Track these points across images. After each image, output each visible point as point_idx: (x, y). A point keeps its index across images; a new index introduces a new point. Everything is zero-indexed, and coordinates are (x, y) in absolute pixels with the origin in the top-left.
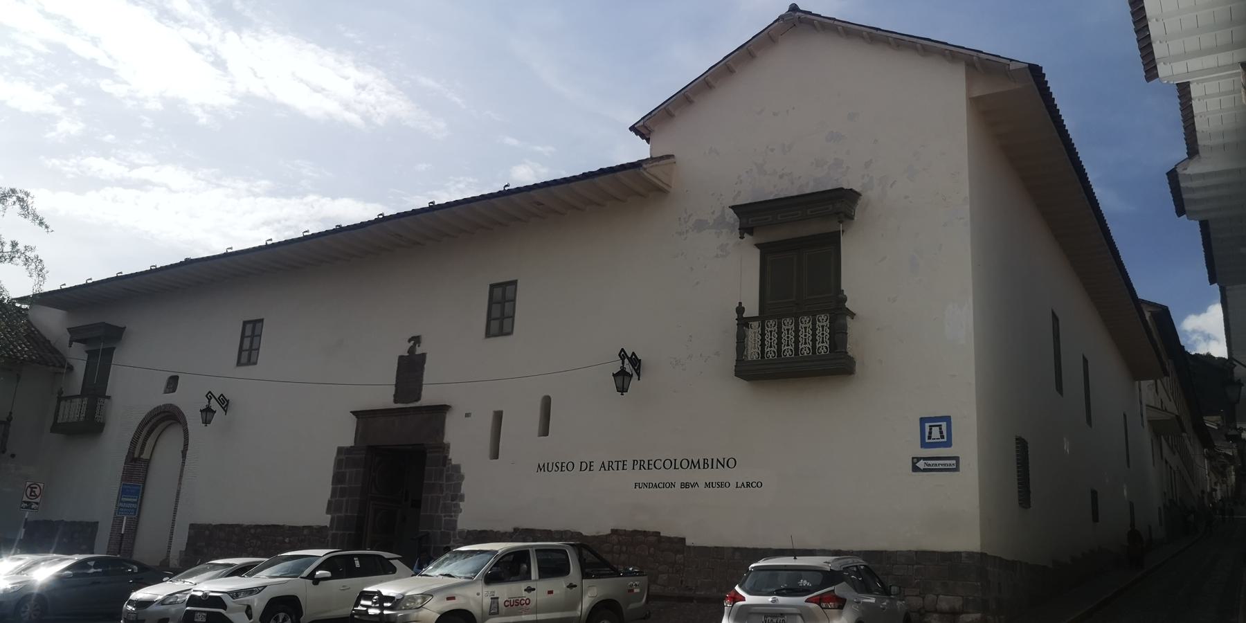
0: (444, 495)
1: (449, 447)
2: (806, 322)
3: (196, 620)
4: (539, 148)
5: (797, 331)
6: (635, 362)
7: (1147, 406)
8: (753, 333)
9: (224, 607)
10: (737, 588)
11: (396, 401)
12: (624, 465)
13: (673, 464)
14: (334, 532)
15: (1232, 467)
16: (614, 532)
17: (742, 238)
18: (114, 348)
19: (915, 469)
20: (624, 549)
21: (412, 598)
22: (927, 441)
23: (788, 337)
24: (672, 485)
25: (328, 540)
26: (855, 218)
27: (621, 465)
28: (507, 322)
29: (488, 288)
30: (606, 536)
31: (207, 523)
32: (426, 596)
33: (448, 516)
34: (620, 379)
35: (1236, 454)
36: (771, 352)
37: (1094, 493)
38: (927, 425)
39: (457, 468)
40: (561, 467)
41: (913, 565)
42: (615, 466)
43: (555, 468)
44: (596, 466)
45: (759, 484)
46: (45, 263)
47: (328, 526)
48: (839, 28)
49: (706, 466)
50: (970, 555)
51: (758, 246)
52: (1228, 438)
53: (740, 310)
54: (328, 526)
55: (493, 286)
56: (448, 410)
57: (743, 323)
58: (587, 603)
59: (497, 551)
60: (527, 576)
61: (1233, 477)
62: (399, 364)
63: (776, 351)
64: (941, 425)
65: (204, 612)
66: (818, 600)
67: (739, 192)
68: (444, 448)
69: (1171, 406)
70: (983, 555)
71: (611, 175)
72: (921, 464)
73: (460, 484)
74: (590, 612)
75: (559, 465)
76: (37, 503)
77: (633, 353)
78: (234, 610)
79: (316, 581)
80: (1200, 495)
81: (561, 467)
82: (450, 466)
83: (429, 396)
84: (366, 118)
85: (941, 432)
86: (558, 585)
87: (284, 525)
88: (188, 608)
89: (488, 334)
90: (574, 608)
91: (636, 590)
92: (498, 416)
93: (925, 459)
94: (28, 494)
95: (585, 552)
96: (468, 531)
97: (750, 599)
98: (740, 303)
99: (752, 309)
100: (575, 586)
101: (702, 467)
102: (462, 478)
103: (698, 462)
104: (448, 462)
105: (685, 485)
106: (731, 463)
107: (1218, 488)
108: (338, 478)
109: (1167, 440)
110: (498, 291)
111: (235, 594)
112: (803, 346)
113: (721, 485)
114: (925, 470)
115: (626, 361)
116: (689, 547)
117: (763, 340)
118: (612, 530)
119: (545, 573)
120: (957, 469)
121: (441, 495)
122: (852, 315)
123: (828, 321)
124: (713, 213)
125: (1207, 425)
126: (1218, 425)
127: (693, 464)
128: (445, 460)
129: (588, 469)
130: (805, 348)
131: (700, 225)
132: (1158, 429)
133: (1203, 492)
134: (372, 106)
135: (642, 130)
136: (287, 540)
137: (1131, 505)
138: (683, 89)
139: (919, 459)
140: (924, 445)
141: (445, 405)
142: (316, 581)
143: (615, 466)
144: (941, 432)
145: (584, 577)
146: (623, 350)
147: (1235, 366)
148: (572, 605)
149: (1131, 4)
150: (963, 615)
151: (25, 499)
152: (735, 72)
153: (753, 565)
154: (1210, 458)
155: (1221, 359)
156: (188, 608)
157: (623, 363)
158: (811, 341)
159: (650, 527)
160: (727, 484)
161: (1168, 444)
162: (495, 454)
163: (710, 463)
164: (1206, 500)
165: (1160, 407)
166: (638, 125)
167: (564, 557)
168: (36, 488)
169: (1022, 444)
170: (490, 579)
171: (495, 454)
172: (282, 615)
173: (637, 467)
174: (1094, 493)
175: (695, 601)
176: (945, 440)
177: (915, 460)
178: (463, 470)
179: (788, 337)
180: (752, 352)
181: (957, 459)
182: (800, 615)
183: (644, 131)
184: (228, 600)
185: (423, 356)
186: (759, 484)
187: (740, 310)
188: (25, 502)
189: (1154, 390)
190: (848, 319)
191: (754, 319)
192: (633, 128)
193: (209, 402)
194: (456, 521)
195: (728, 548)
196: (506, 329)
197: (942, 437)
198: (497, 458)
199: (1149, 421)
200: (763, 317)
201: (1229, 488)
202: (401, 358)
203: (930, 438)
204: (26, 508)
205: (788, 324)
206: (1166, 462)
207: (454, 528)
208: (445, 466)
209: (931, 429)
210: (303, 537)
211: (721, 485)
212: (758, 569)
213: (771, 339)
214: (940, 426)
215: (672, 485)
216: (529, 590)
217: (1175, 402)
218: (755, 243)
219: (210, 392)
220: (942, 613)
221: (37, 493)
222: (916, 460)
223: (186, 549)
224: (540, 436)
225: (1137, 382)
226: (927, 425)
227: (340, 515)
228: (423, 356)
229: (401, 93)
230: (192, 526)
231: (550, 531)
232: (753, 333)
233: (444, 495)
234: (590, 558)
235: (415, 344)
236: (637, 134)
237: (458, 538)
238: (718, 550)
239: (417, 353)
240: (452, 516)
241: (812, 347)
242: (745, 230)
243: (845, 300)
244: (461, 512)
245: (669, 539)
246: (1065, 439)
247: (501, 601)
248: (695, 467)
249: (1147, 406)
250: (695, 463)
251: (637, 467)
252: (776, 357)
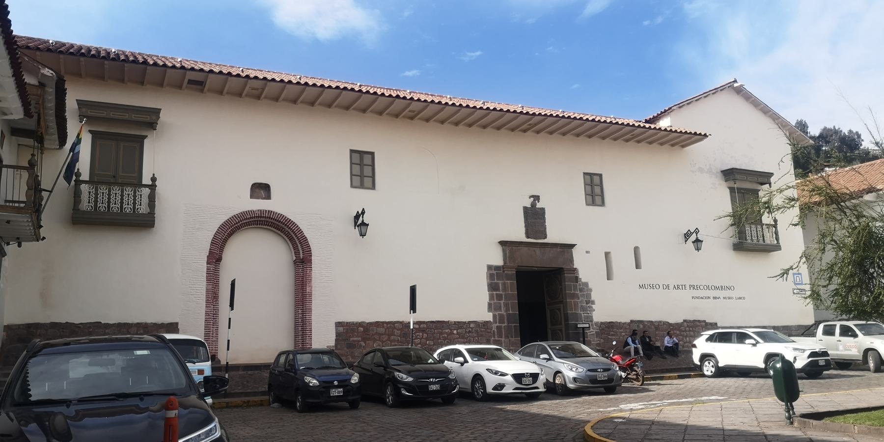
0: (580, 300)
13: (708, 287)
14: (498, 324)
16: (685, 321)
18: (146, 137)
20: (691, 329)
24: (709, 298)
25: (494, 331)
27: (683, 287)
30: (682, 323)
33: (586, 313)
38: (795, 276)
39: (586, 284)
40: (652, 287)
42: (681, 287)
43: (649, 287)
47: (492, 321)
54: (492, 321)
63: (132, 208)
73: (590, 294)
75: (651, 286)
81: (652, 287)
82: (581, 283)
96: (601, 322)
98: (154, 175)
102: (591, 290)
104: (579, 280)
105: (715, 298)
112: (126, 206)
118: (631, 321)
123: (107, 190)
127: (716, 288)
128: (577, 279)
136: (455, 332)
139: (794, 289)
143: (681, 287)
158: (98, 201)
163: (723, 288)
173: (692, 288)
178: (590, 286)
185: (543, 210)
193: (697, 236)
194: (592, 316)
210: (470, 329)
215: (709, 298)
219: (697, 228)
223: (335, 344)
227: (500, 313)
230: (338, 324)
231: (652, 321)
233: (580, 300)
237: (595, 326)
241: (121, 206)
252: (93, 210)
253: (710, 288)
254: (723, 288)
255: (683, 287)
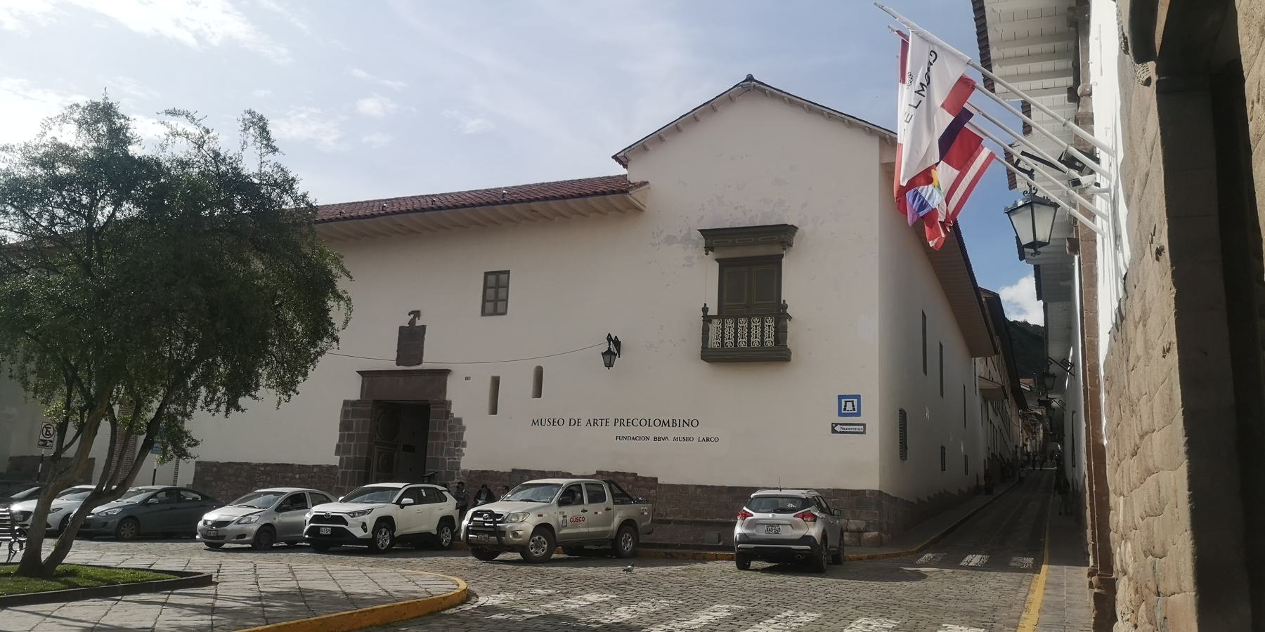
1: (451, 404)
2: (756, 322)
3: (321, 533)
4: (389, 82)
5: (749, 328)
6: (617, 343)
7: (980, 377)
8: (715, 326)
9: (346, 523)
10: (745, 508)
11: (398, 364)
12: (606, 422)
13: (648, 423)
15: (1041, 425)
17: (707, 254)
19: (834, 431)
21: (517, 515)
22: (843, 412)
23: (743, 332)
25: (338, 477)
26: (793, 245)
27: (604, 422)
28: (500, 305)
29: (483, 275)
31: (215, 461)
32: (526, 513)
34: (608, 357)
35: (1044, 413)
36: (729, 342)
37: (943, 448)
38: (843, 401)
39: (459, 421)
41: (831, 499)
42: (599, 422)
44: (583, 422)
45: (717, 439)
46: (352, 302)
47: (338, 465)
48: (786, 99)
49: (675, 425)
50: (872, 492)
51: (717, 260)
52: (1041, 403)
53: (705, 309)
54: (338, 465)
55: (487, 274)
56: (448, 373)
57: (707, 319)
58: (617, 521)
59: (562, 485)
60: (581, 502)
61: (1041, 435)
62: (400, 332)
64: (853, 401)
65: (329, 527)
66: (803, 516)
67: (702, 217)
68: (446, 405)
69: (996, 376)
70: (880, 492)
71: (602, 197)
72: (838, 428)
73: (463, 434)
74: (620, 526)
76: (51, 441)
77: (616, 337)
78: (354, 526)
79: (402, 506)
80: (1014, 449)
83: (431, 359)
84: (199, 37)
85: (853, 406)
86: (600, 508)
87: (293, 464)
88: (312, 524)
89: (484, 313)
90: (610, 525)
91: (646, 513)
92: (496, 382)
93: (841, 424)
94: (44, 434)
95: (613, 485)
96: (471, 471)
97: (756, 515)
98: (705, 304)
99: (713, 311)
100: (610, 509)
101: (671, 425)
102: (464, 428)
103: (668, 421)
105: (656, 439)
106: (695, 423)
107: (1028, 443)
108: (345, 426)
109: (992, 404)
110: (492, 278)
111: (353, 514)
113: (686, 439)
114: (840, 432)
115: (611, 342)
116: (661, 485)
117: (723, 333)
119: (591, 500)
120: (864, 433)
121: (445, 442)
122: (790, 318)
124: (681, 231)
125: (1022, 386)
126: (1030, 387)
127: (664, 423)
128: (448, 414)
129: (576, 424)
130: (756, 342)
131: (670, 240)
132: (987, 396)
133: (1016, 447)
134: (206, 24)
135: (621, 159)
136: (297, 476)
137: (966, 457)
138: (659, 130)
139: (836, 424)
140: (840, 414)
141: (447, 370)
142: (402, 506)
143: (599, 422)
144: (853, 406)
145: (615, 503)
146: (609, 335)
147: (1051, 363)
148: (609, 521)
149: (974, 4)
150: (866, 533)
151: (42, 437)
152: (700, 121)
153: (754, 495)
154: (1023, 417)
155: (1036, 327)
156: (312, 524)
157: (610, 345)
159: (629, 470)
160: (692, 439)
161: (993, 407)
162: (494, 410)
163: (678, 422)
164: (1019, 455)
165: (988, 378)
166: (619, 155)
167: (601, 490)
168: (50, 428)
169: (903, 414)
170: (561, 503)
171: (494, 410)
172: (384, 530)
173: (618, 424)
174: (943, 448)
175: (672, 524)
176: (856, 412)
177: (834, 425)
178: (464, 423)
179: (743, 332)
180: (714, 342)
181: (864, 425)
182: (790, 525)
183: (624, 160)
184: (347, 517)
186: (717, 439)
187: (705, 309)
188: (42, 440)
189: (985, 363)
190: (788, 320)
191: (714, 317)
192: (615, 157)
195: (691, 486)
196: (500, 309)
197: (854, 410)
198: (496, 414)
199: (980, 389)
200: (722, 315)
201: (1038, 444)
202: (402, 328)
203: (845, 410)
204: (43, 445)
205: (743, 323)
206: (991, 422)
207: (458, 469)
208: (448, 419)
209: (846, 404)
211: (686, 439)
212: (756, 497)
213: (729, 333)
214: (853, 401)
216: (584, 511)
217: (999, 371)
218: (715, 258)
220: (852, 532)
221: (52, 433)
222: (834, 425)
223: (194, 483)
224: (533, 397)
225: (973, 359)
226: (843, 401)
228: (424, 327)
229: (239, 13)
232: (715, 326)
234: (617, 491)
235: (414, 317)
236: (616, 161)
238: (684, 488)
239: (417, 325)
240: (455, 459)
242: (709, 248)
243: (786, 307)
244: (464, 455)
245: (644, 479)
246: (927, 409)
247: (568, 519)
248: (665, 425)
249: (980, 377)
250: (666, 422)
251: (618, 424)
253: (652, 424)
254: (678, 422)
255: (604, 422)
